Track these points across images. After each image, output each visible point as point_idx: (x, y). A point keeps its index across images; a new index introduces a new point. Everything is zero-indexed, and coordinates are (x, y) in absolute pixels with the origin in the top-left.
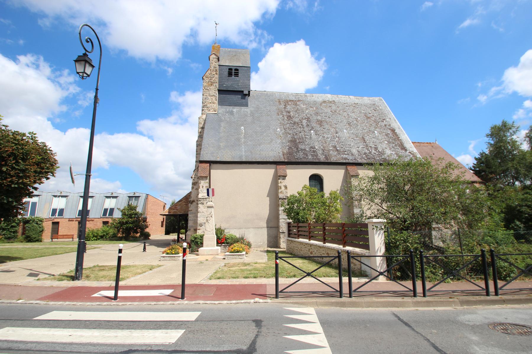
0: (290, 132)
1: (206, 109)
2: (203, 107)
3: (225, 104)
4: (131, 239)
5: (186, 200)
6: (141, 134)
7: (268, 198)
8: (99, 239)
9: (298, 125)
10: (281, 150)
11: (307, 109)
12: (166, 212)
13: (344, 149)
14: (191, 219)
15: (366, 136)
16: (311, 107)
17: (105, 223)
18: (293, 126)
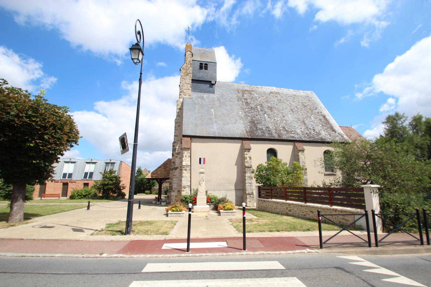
0: (249, 115)
1: (182, 94)
2: (180, 92)
3: (197, 91)
4: (112, 198)
5: (164, 167)
6: (97, 112)
7: (236, 167)
8: (82, 198)
9: (254, 110)
10: (244, 129)
11: (259, 97)
12: (149, 176)
13: (291, 129)
14: (175, 182)
15: (306, 120)
16: (262, 96)
17: (86, 185)
18: (251, 110)
